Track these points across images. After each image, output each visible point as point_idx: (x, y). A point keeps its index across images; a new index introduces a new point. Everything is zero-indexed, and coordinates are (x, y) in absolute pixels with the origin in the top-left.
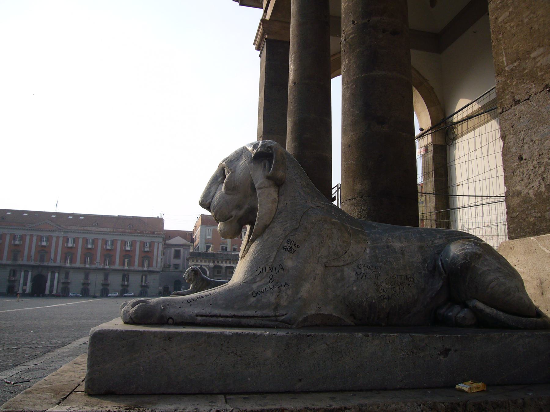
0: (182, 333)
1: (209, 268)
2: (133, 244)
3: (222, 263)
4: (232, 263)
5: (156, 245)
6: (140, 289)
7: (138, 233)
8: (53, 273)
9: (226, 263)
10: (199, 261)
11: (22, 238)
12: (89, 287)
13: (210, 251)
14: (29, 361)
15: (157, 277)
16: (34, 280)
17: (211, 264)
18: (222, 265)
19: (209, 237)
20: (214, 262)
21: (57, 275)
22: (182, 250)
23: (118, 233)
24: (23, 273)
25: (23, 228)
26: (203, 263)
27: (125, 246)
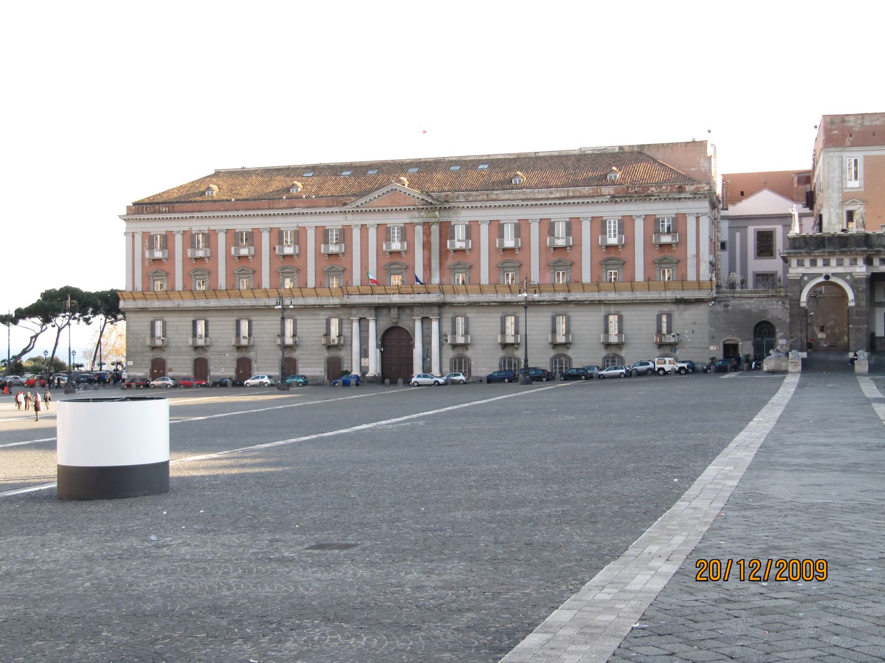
0: (367, 423)
1: (854, 283)
2: (520, 228)
5: (691, 222)
8: (425, 320)
10: (820, 262)
11: (344, 234)
13: (854, 229)
15: (700, 313)
16: (384, 340)
17: (861, 269)
19: (853, 184)
20: (869, 262)
21: (435, 325)
22: (779, 230)
24: (356, 326)
25: (343, 209)
27: (604, 233)
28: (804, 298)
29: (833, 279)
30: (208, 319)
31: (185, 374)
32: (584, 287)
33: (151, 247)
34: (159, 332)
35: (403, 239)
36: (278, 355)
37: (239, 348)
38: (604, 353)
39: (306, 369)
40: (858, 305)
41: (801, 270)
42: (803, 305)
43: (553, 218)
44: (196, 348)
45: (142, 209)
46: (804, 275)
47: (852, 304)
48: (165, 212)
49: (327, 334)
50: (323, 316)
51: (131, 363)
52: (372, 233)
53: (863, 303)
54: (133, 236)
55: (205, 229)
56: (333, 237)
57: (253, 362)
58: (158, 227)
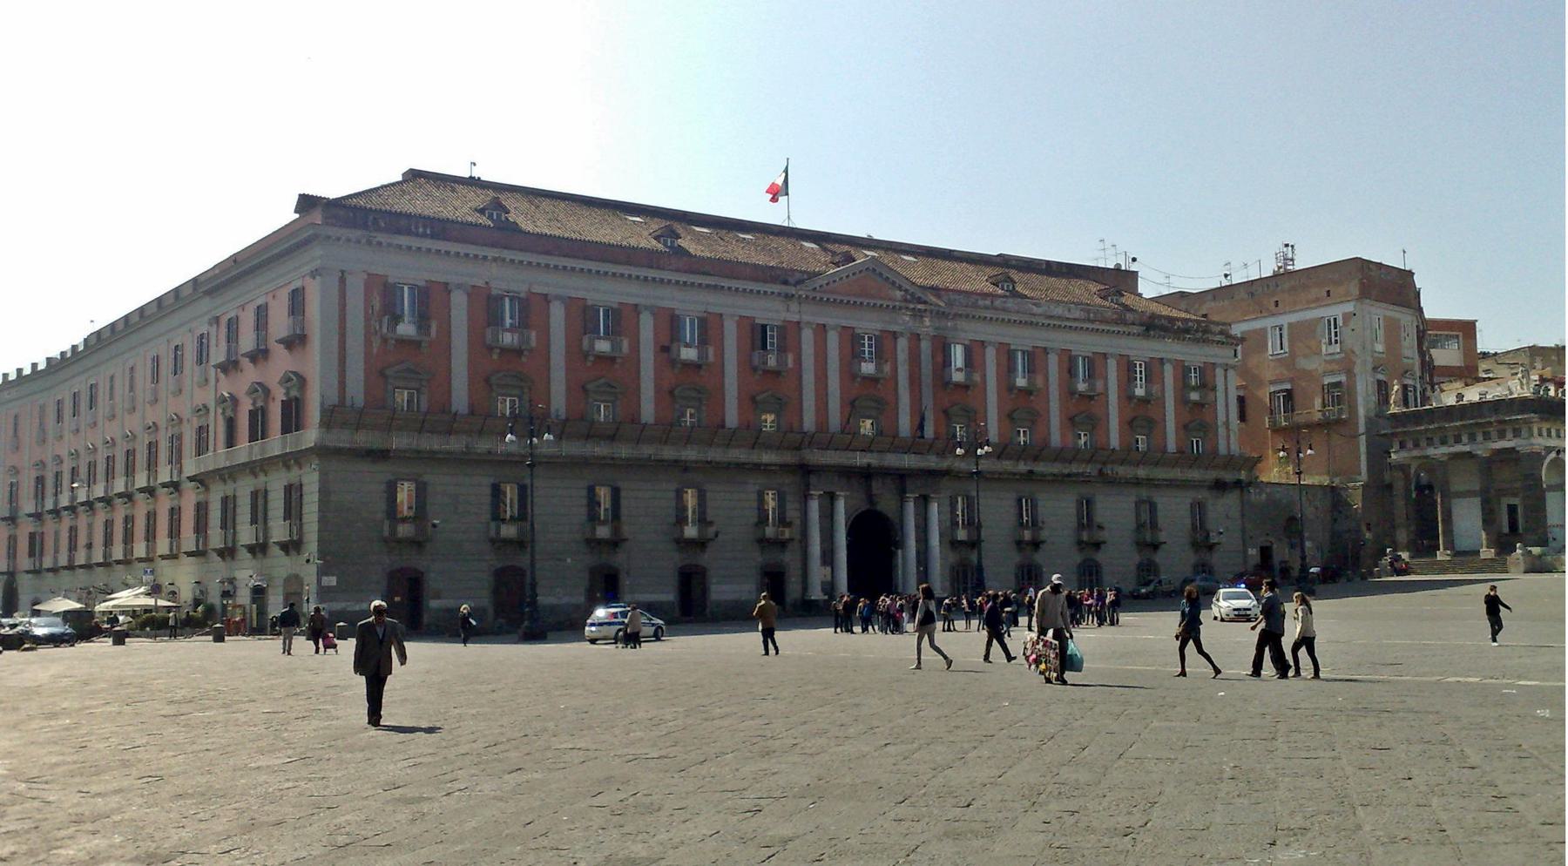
8: (924, 501)
30: (620, 484)
31: (574, 600)
32: (641, 434)
34: (510, 508)
36: (673, 560)
39: (725, 587)
43: (1076, 350)
48: (424, 235)
50: (753, 484)
51: (331, 581)
52: (833, 339)
54: (342, 280)
55: (522, 289)
56: (772, 339)
57: (622, 576)
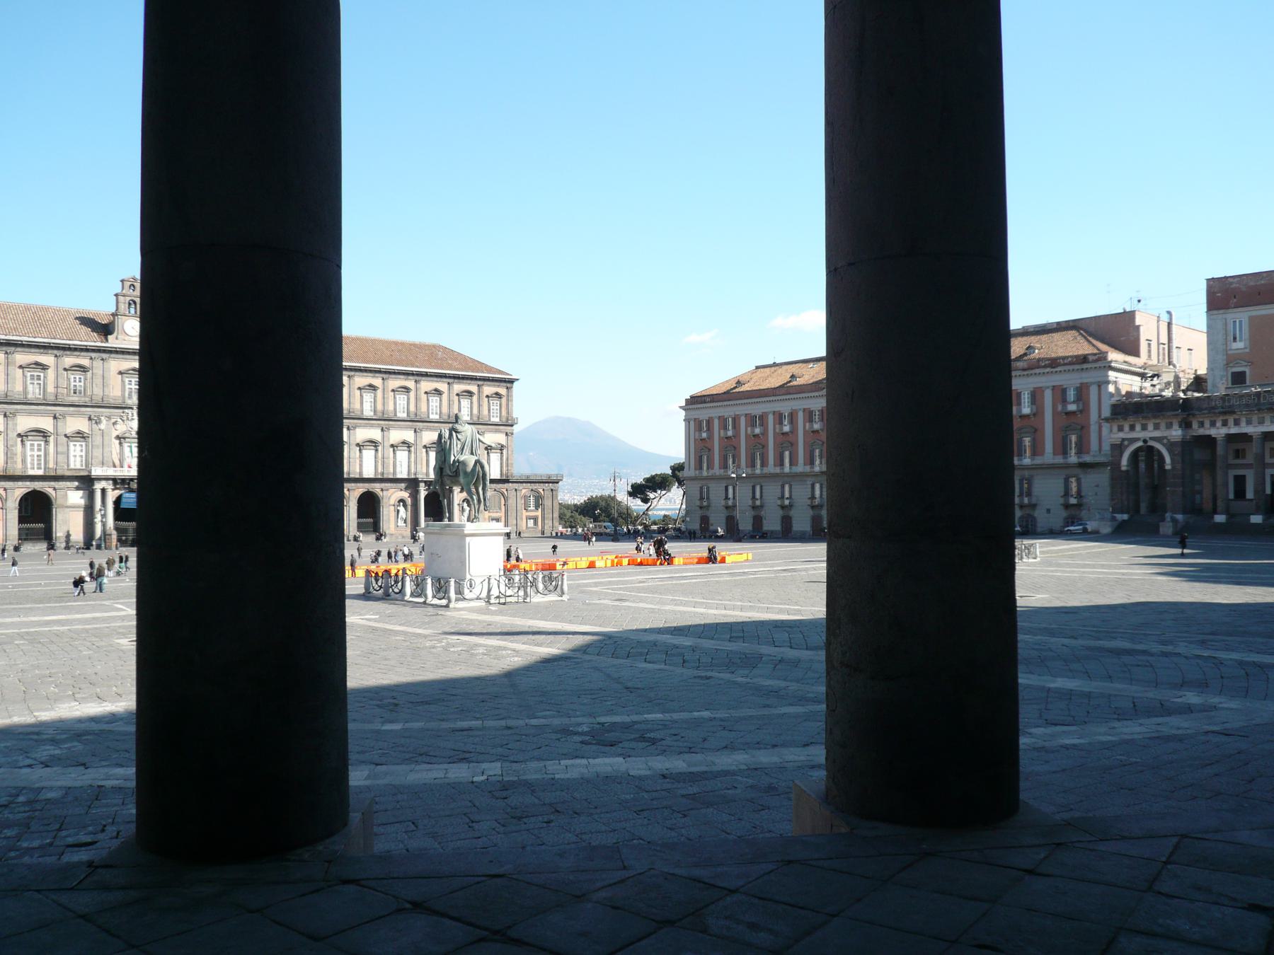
1: (1171, 446)
3: (1213, 424)
4: (1243, 424)
6: (811, 512)
7: (1045, 367)
9: (1225, 424)
10: (1138, 427)
12: (1037, 513)
14: (1119, 720)
17: (1176, 433)
18: (1213, 432)
20: (1186, 425)
23: (1037, 371)
26: (1151, 433)
28: (1124, 461)
29: (1151, 443)
33: (811, 421)
35: (762, 425)
37: (754, 507)
38: (1064, 514)
40: (1173, 468)
41: (1122, 435)
42: (1124, 468)
44: (727, 507)
45: (694, 402)
46: (1123, 440)
47: (1168, 467)
49: (813, 497)
53: (1179, 466)
58: (704, 414)
